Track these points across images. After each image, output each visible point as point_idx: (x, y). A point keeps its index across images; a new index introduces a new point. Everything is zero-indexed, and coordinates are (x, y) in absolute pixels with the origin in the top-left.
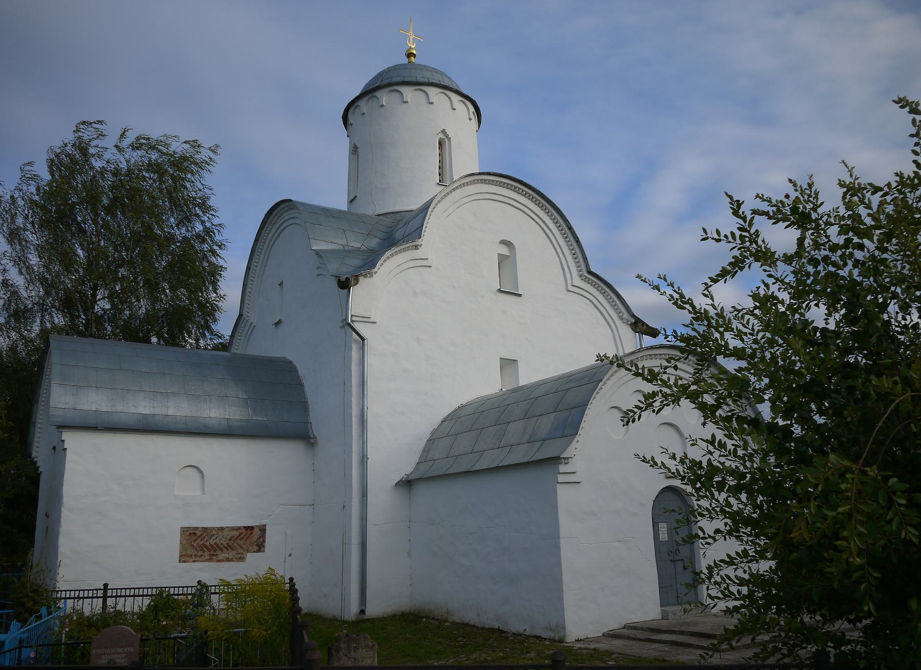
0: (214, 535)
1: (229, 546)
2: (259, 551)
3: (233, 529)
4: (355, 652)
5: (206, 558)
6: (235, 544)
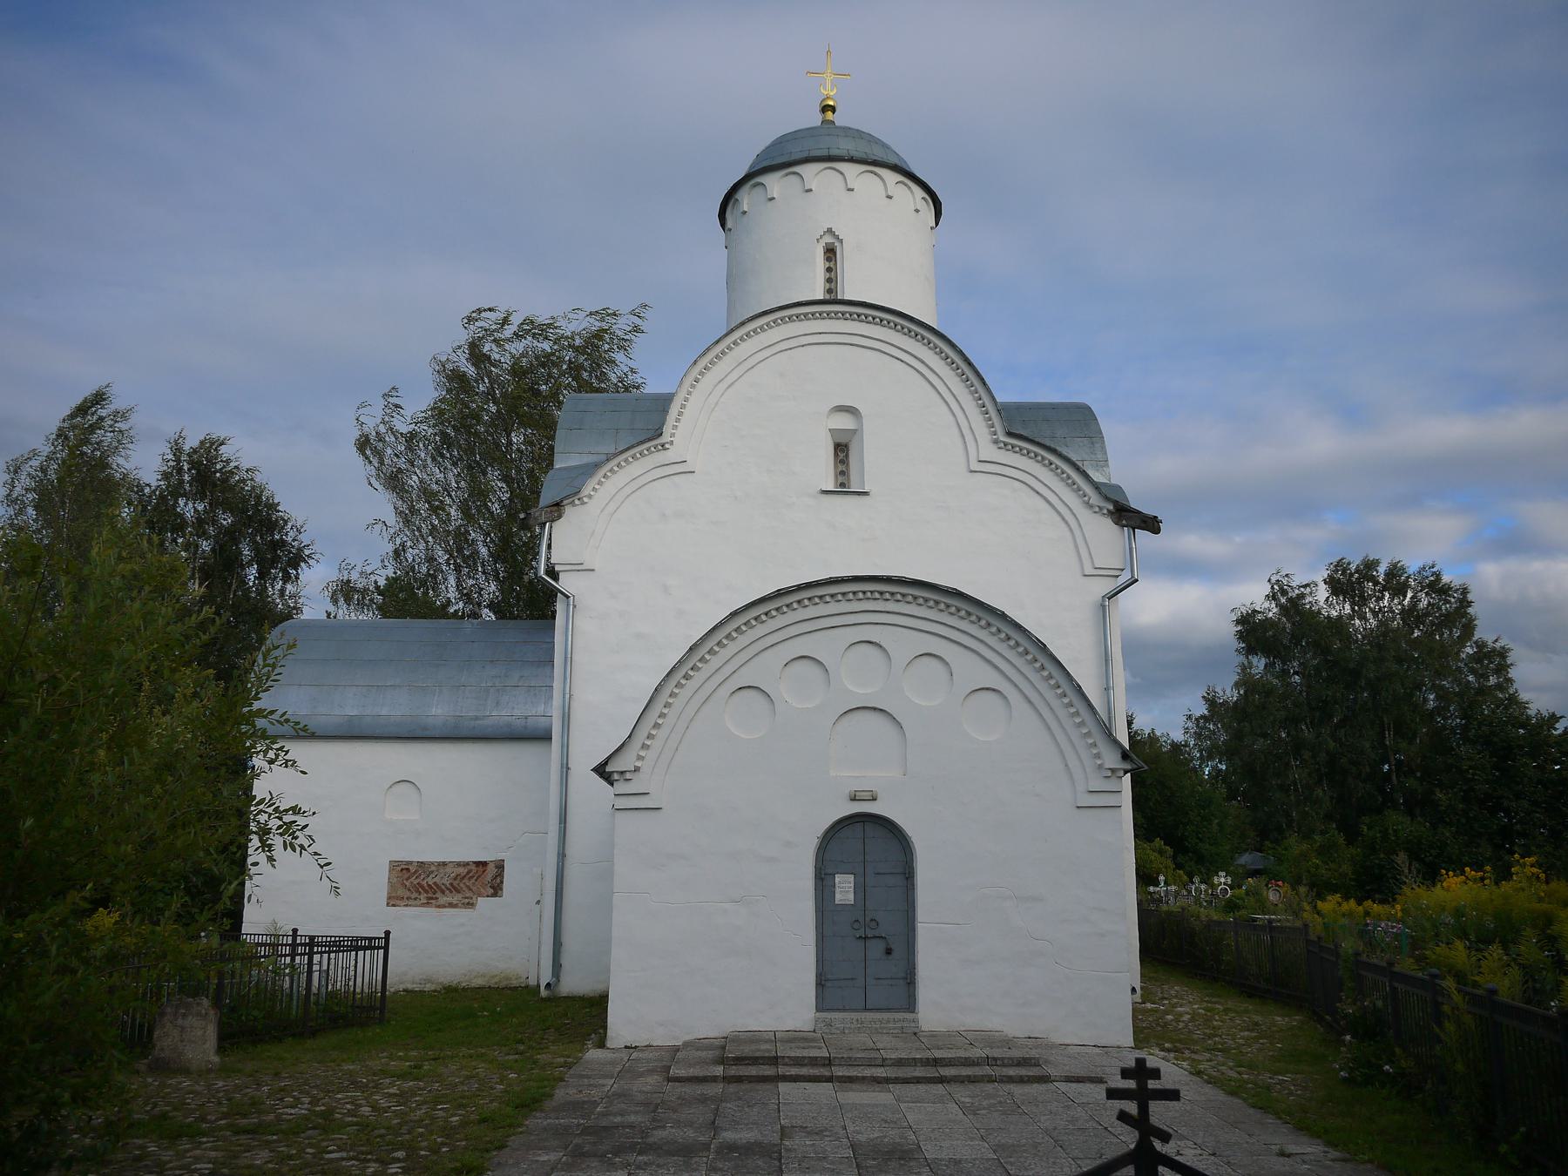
0: (432, 872)
1: (454, 887)
2: (495, 895)
3: (459, 864)
4: (183, 1019)
5: (422, 902)
6: (462, 885)
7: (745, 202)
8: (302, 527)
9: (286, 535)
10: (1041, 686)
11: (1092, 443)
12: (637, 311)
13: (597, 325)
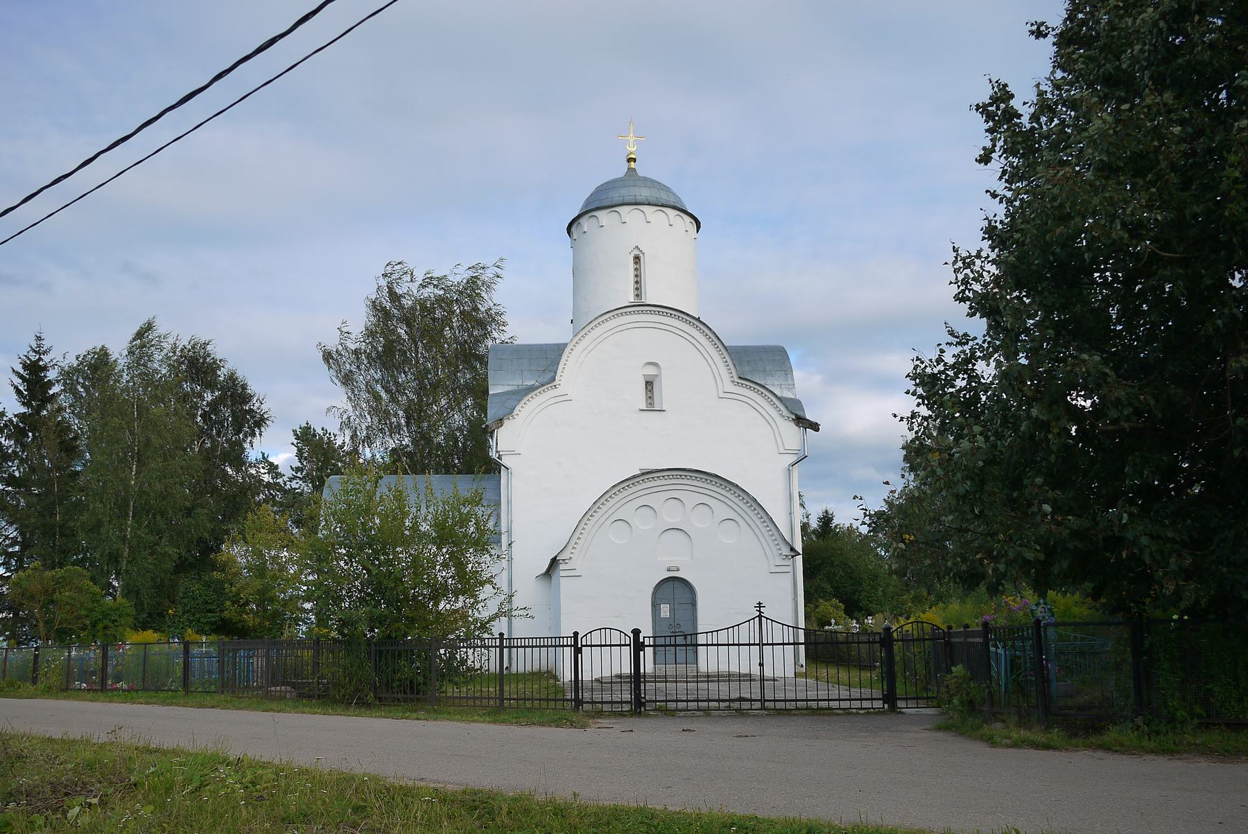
7: (585, 226)
8: (263, 400)
9: (253, 405)
10: (754, 517)
11: (786, 374)
12: (497, 264)
13: (471, 273)
